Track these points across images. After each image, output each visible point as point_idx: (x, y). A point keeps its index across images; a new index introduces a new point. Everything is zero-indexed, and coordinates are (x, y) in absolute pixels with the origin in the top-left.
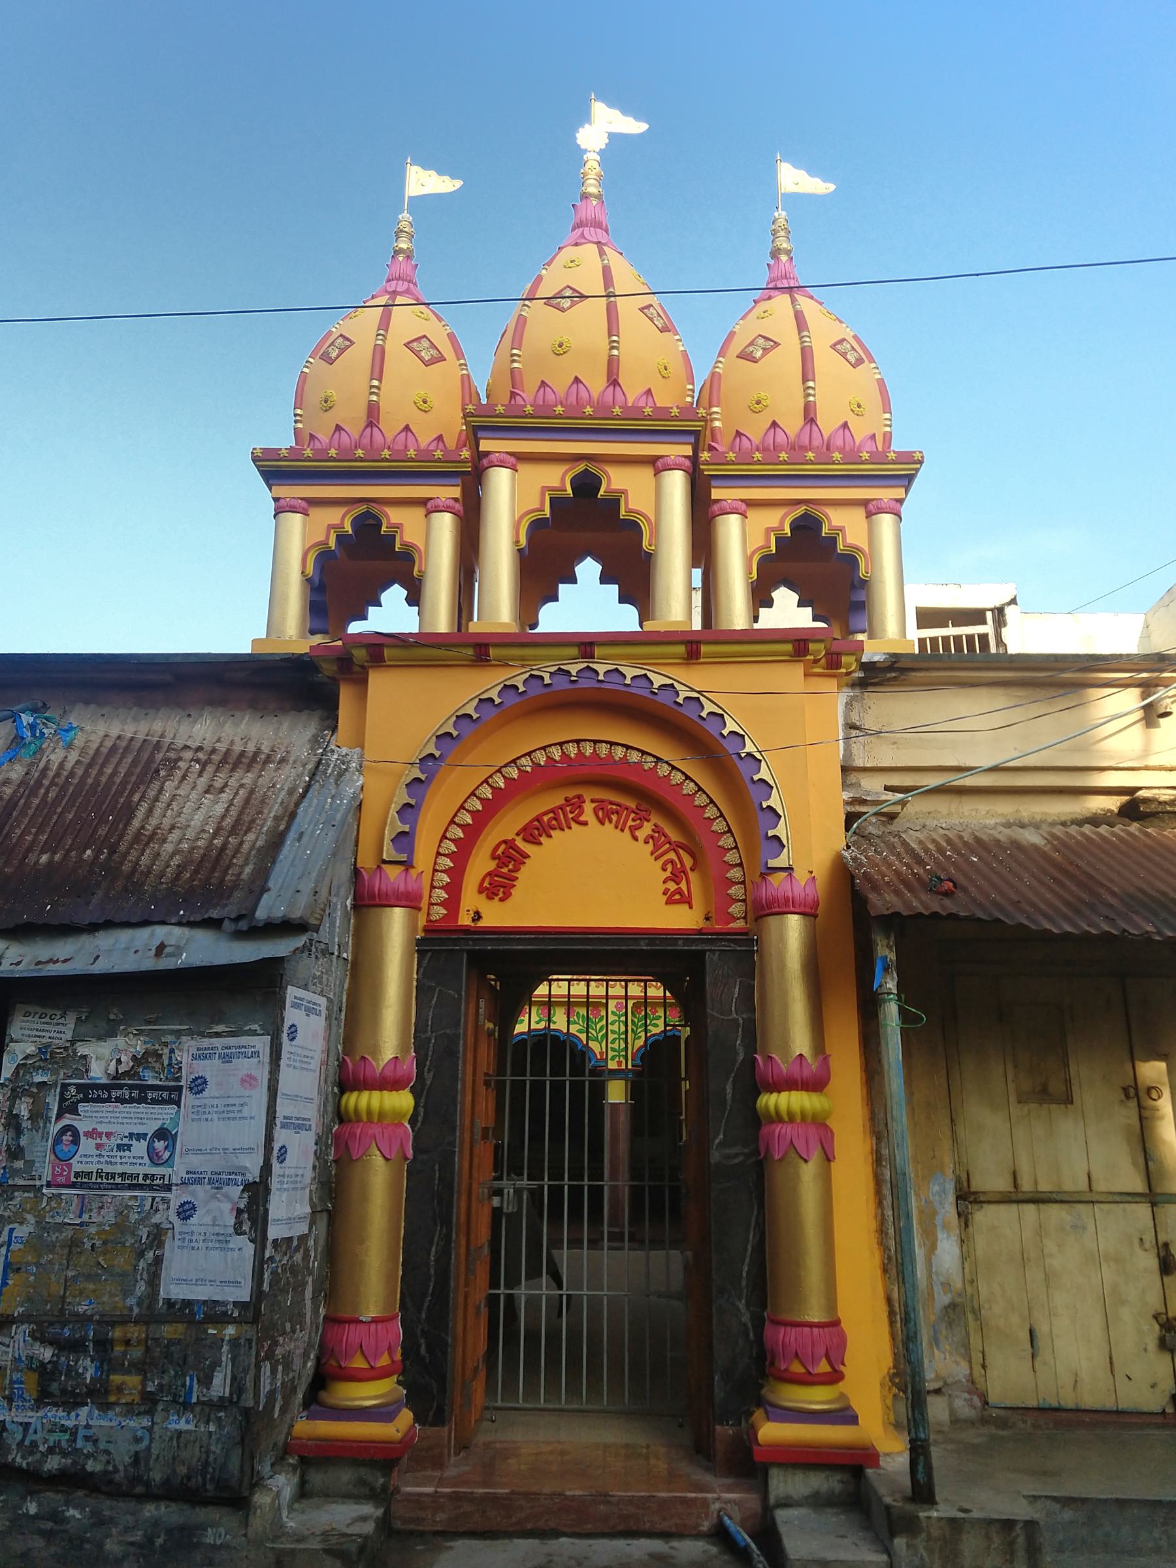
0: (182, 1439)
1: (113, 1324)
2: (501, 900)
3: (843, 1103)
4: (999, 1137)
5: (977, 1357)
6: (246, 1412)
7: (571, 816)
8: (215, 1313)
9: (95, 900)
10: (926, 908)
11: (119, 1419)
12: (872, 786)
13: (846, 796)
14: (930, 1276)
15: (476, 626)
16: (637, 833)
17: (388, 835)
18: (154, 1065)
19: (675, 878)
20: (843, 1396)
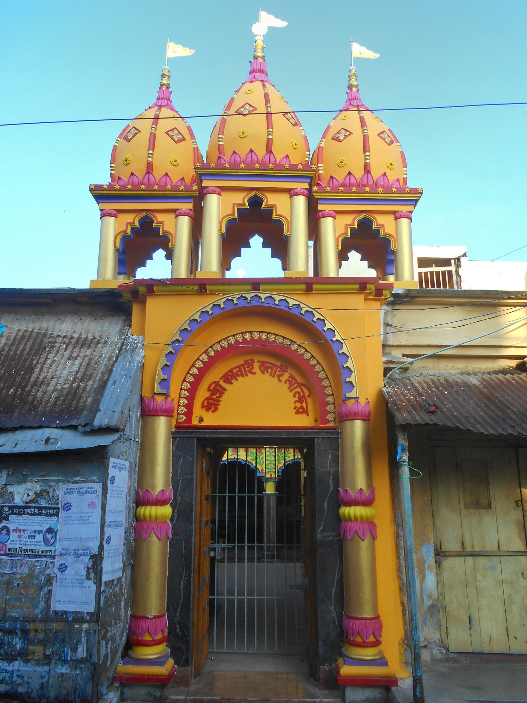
0: (64, 677)
1: (29, 622)
2: (213, 411)
3: (380, 512)
4: (456, 524)
5: (444, 630)
6: (94, 665)
7: (247, 369)
8: (78, 618)
9: (15, 415)
10: (423, 421)
11: (33, 667)
12: (397, 354)
13: (384, 359)
14: (422, 592)
15: (200, 274)
16: (281, 378)
17: (157, 380)
18: (45, 497)
19: (300, 401)
20: (381, 652)
